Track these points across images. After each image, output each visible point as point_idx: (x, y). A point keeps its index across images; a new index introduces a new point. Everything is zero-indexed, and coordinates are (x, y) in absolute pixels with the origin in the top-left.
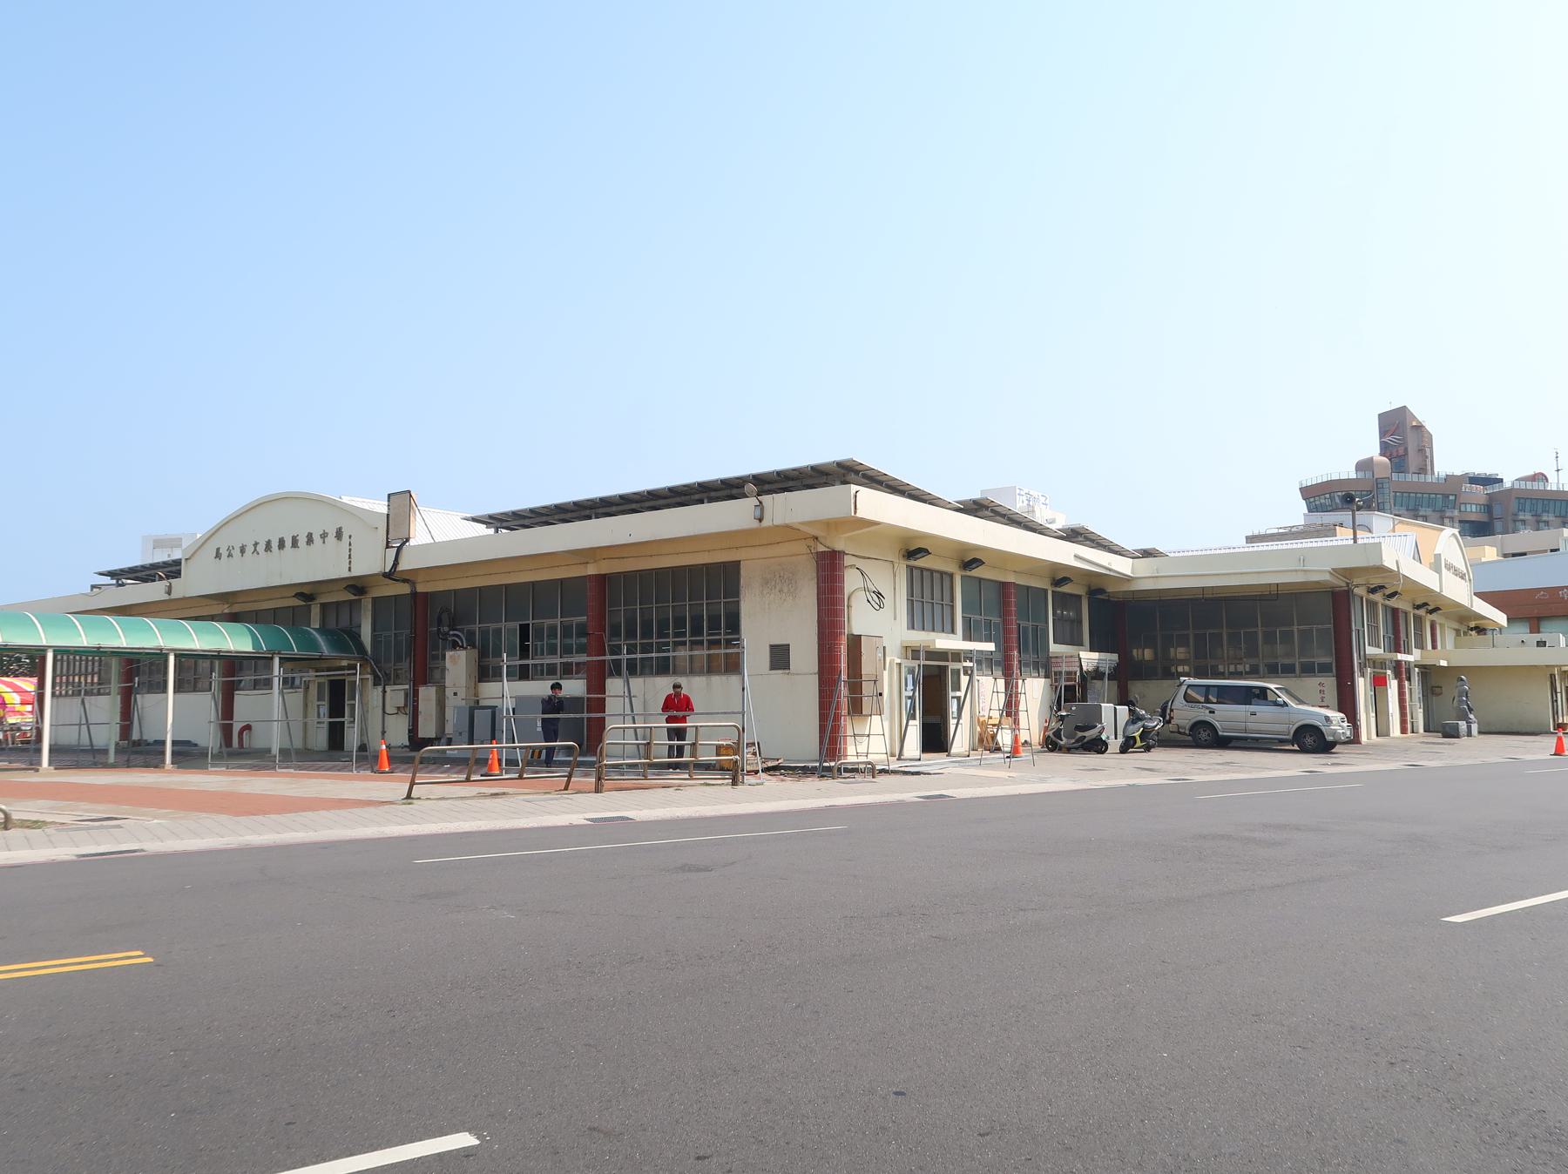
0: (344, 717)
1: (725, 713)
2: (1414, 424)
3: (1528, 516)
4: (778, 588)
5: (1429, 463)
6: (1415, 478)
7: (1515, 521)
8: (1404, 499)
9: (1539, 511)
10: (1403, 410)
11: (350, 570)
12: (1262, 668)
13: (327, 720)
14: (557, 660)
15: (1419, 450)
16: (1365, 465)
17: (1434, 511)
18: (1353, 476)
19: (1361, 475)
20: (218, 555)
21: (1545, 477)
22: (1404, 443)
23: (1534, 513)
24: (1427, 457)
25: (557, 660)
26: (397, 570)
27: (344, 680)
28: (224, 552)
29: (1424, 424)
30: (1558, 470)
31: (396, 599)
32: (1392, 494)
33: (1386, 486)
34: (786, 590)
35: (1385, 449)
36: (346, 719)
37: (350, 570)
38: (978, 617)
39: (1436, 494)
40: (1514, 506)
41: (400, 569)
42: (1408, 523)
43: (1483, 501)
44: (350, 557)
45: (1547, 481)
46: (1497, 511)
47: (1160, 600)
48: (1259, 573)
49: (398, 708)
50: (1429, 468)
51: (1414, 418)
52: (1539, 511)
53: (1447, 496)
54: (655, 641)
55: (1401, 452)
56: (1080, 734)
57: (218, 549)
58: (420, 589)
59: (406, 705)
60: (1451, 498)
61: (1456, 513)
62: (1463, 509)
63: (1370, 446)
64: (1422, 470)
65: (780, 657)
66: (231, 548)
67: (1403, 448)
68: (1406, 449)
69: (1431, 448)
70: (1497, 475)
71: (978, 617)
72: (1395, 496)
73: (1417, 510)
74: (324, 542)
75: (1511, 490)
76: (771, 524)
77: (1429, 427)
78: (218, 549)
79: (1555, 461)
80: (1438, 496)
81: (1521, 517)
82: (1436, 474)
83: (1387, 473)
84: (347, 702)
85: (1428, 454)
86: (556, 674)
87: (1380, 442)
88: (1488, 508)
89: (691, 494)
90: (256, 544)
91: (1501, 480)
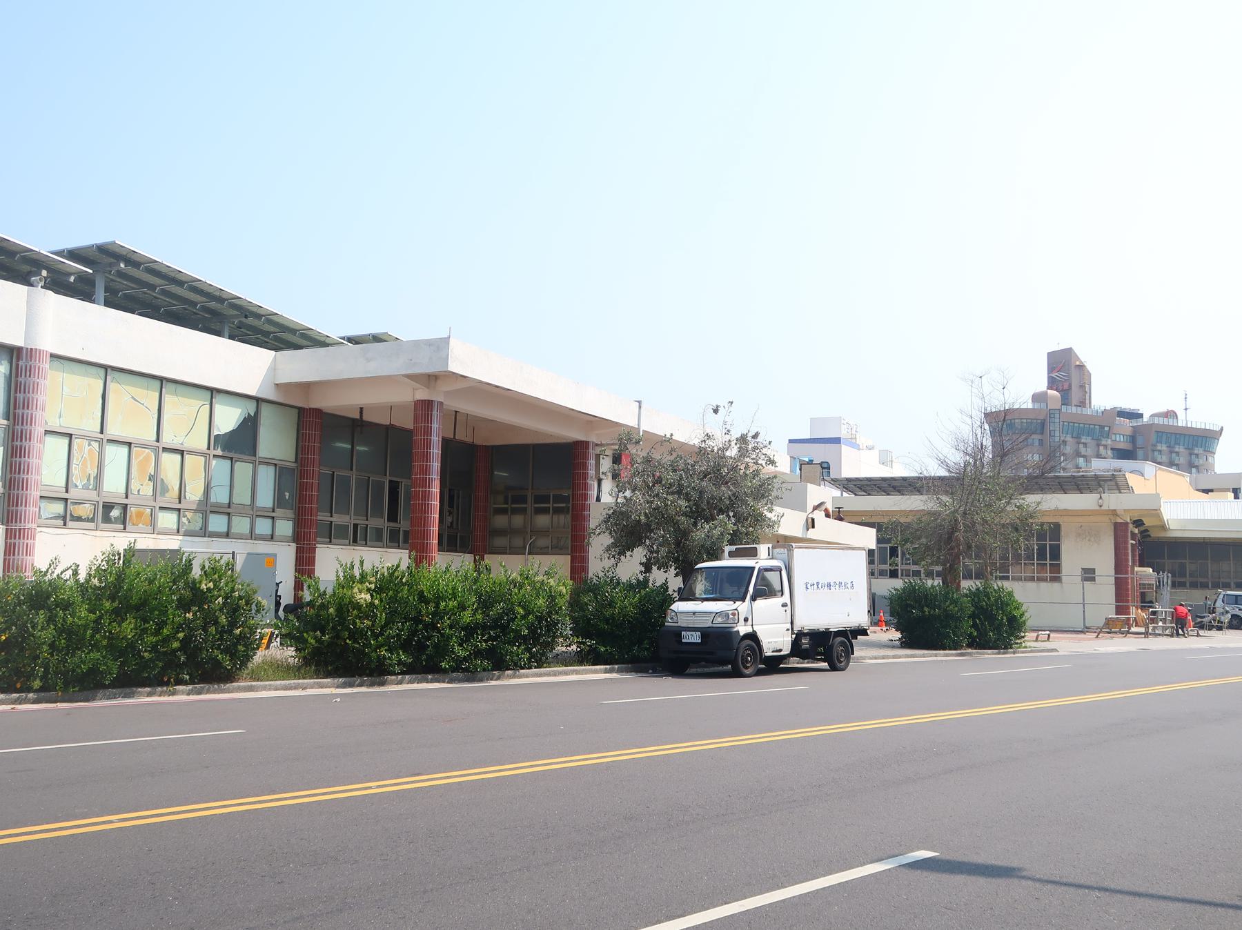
2: (1078, 363)
3: (1163, 447)
4: (1087, 538)
5: (1087, 398)
6: (1074, 410)
7: (1154, 451)
8: (1070, 427)
9: (1172, 443)
10: (1068, 352)
12: (1232, 584)
15: (1081, 386)
16: (1037, 398)
17: (1092, 439)
18: (1030, 406)
19: (1037, 406)
21: (1176, 414)
22: (1069, 379)
23: (1168, 445)
24: (1086, 392)
29: (1085, 364)
30: (1186, 409)
32: (1061, 423)
33: (1057, 416)
34: (1092, 539)
35: (1052, 383)
38: (346, 473)
39: (1095, 425)
40: (1154, 438)
42: (1164, 470)
43: (1129, 432)
45: (1177, 418)
46: (1140, 442)
47: (1175, 542)
48: (1237, 531)
50: (1087, 402)
51: (1078, 359)
52: (1172, 443)
53: (1102, 427)
54: (1048, 562)
55: (1066, 387)
56: (1199, 620)
60: (1106, 429)
61: (1109, 442)
62: (1114, 439)
63: (1040, 383)
64: (1083, 403)
65: (1089, 575)
67: (1068, 383)
68: (1070, 386)
69: (1090, 385)
70: (1139, 410)
71: (346, 473)
72: (1063, 425)
73: (1080, 438)
75: (1149, 426)
76: (1107, 508)
77: (1089, 367)
79: (1184, 402)
80: (1096, 427)
81: (1159, 448)
82: (1092, 407)
83: (1057, 405)
85: (1087, 390)
87: (1049, 377)
88: (1133, 439)
91: (1141, 416)
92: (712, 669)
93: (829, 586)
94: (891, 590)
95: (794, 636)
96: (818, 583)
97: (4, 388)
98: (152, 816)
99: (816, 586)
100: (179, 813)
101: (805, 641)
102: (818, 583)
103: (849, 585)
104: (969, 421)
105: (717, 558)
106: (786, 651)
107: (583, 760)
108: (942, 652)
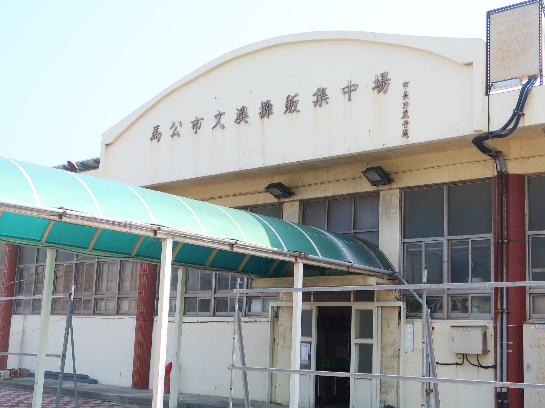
0: (348, 370)
1: (213, 321)
11: (405, 134)
13: (313, 372)
14: (210, 295)
20: (156, 135)
25: (210, 295)
26: (520, 125)
27: (350, 308)
28: (166, 132)
31: (449, 189)
36: (353, 373)
37: (405, 134)
41: (527, 124)
44: (405, 114)
49: (465, 356)
57: (156, 129)
58: (513, 168)
59: (485, 351)
66: (177, 124)
74: (350, 99)
78: (156, 129)
84: (354, 341)
86: (84, 300)
89: (306, 201)
90: (219, 115)
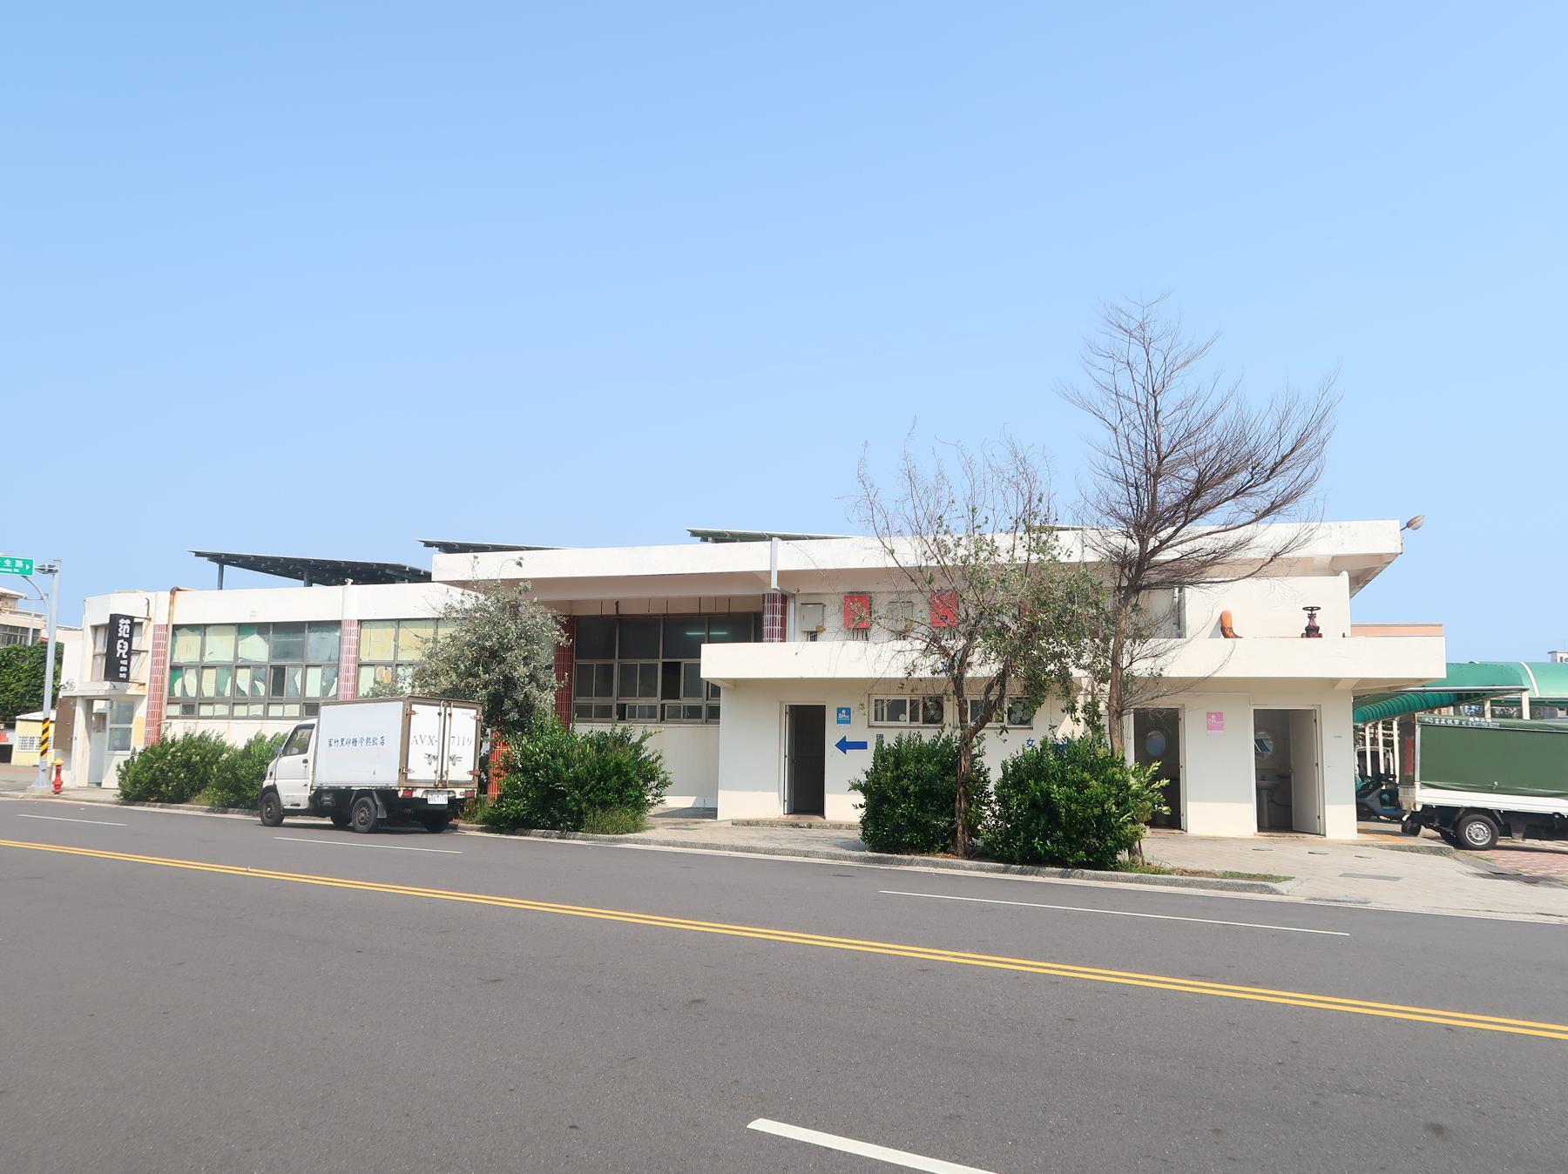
92: (412, 829)
93: (355, 741)
94: (216, 732)
95: (313, 792)
96: (342, 740)
97: (328, 632)
98: (1459, 1019)
99: (340, 743)
100: (1378, 1009)
101: (327, 799)
102: (342, 740)
103: (378, 741)
104: (1137, 352)
105: (1365, 752)
106: (304, 805)
107: (986, 960)
108: (918, 858)
